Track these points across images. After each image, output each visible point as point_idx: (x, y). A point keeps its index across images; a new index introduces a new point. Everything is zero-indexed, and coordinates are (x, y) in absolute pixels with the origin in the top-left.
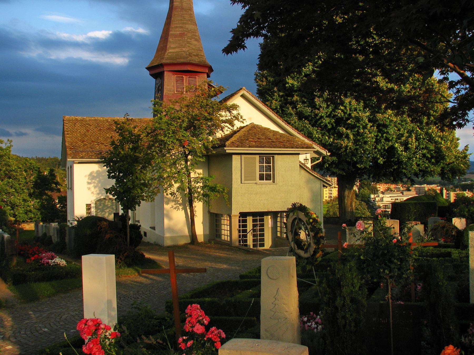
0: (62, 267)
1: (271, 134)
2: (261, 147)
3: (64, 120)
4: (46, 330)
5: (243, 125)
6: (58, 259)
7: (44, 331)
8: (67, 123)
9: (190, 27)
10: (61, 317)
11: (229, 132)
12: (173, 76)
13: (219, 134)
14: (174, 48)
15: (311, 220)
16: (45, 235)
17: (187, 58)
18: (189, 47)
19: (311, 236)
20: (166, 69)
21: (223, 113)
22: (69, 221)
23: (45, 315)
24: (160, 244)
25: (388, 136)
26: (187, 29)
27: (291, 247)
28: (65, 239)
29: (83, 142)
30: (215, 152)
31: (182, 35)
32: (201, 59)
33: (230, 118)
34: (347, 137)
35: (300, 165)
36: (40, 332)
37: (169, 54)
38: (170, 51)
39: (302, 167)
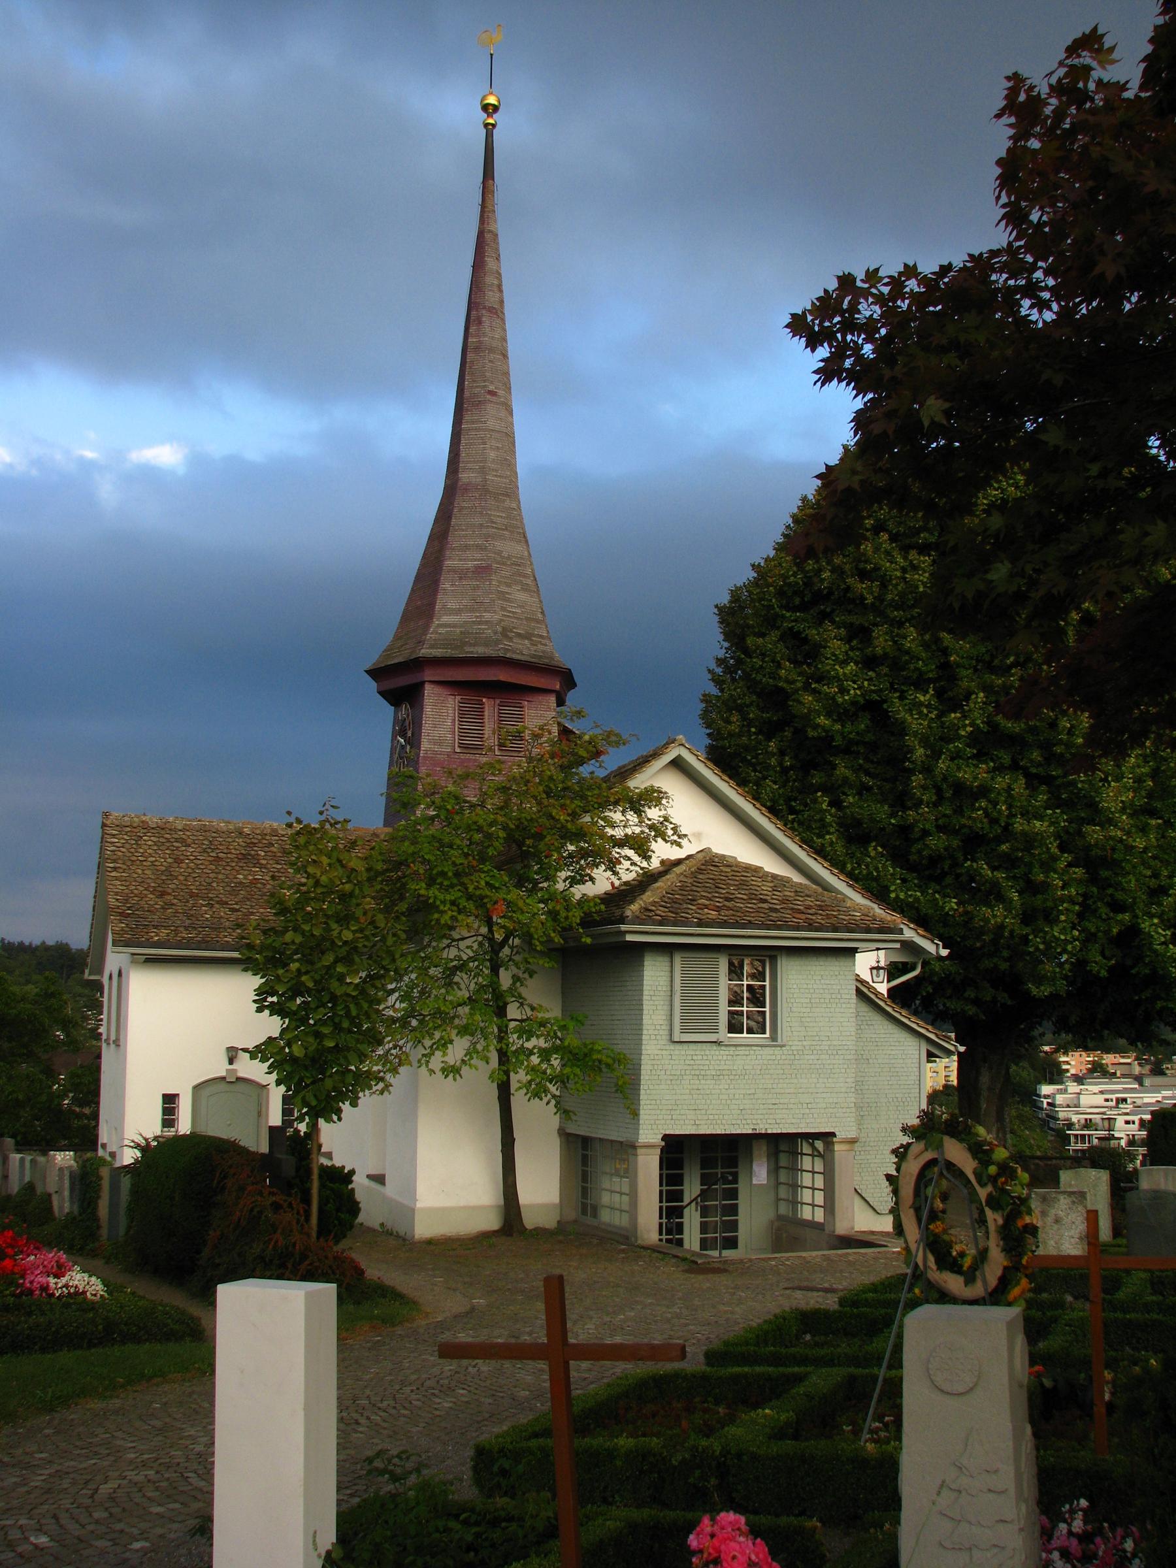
0: (93, 1302)
1: (766, 887)
3: (104, 825)
4: (43, 1540)
5: (674, 853)
6: (79, 1276)
7: (36, 1546)
8: (114, 836)
9: (510, 548)
10: (97, 1489)
11: (633, 876)
13: (602, 882)
14: (458, 612)
15: (993, 1169)
16: (30, 1188)
17: (497, 642)
18: (503, 609)
19: (992, 1227)
20: (429, 674)
21: (617, 816)
22: (104, 1146)
23: (37, 1481)
24: (402, 1234)
25: (1119, 896)
26: (499, 553)
27: (916, 1265)
28: (96, 1205)
29: (162, 894)
30: (589, 940)
31: (482, 571)
33: (637, 830)
34: (1001, 898)
35: (858, 990)
36: (20, 1549)
37: (441, 630)
39: (864, 994)
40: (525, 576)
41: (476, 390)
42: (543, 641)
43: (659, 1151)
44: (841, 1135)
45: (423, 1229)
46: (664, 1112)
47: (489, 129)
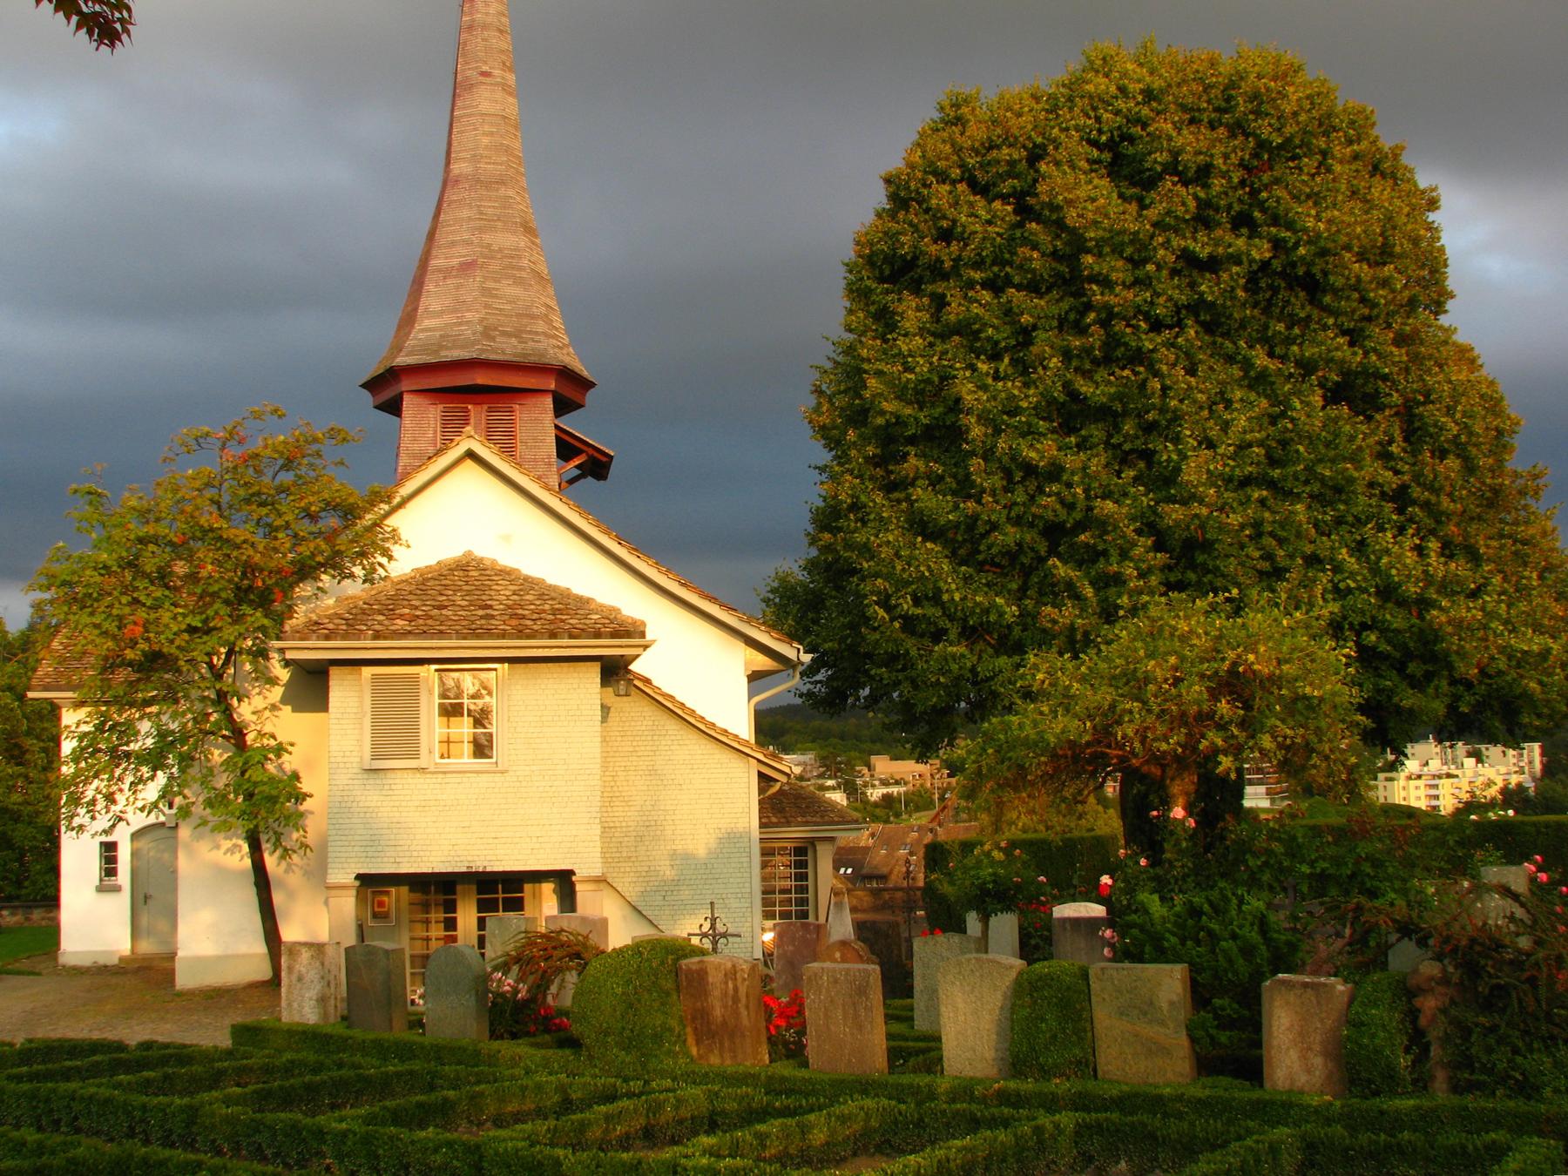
2: (424, 634)
12: (432, 408)
20: (406, 385)
37: (421, 336)
38: (427, 323)
40: (521, 269)
41: (469, 73)
43: (354, 892)
44: (581, 872)
45: (185, 979)
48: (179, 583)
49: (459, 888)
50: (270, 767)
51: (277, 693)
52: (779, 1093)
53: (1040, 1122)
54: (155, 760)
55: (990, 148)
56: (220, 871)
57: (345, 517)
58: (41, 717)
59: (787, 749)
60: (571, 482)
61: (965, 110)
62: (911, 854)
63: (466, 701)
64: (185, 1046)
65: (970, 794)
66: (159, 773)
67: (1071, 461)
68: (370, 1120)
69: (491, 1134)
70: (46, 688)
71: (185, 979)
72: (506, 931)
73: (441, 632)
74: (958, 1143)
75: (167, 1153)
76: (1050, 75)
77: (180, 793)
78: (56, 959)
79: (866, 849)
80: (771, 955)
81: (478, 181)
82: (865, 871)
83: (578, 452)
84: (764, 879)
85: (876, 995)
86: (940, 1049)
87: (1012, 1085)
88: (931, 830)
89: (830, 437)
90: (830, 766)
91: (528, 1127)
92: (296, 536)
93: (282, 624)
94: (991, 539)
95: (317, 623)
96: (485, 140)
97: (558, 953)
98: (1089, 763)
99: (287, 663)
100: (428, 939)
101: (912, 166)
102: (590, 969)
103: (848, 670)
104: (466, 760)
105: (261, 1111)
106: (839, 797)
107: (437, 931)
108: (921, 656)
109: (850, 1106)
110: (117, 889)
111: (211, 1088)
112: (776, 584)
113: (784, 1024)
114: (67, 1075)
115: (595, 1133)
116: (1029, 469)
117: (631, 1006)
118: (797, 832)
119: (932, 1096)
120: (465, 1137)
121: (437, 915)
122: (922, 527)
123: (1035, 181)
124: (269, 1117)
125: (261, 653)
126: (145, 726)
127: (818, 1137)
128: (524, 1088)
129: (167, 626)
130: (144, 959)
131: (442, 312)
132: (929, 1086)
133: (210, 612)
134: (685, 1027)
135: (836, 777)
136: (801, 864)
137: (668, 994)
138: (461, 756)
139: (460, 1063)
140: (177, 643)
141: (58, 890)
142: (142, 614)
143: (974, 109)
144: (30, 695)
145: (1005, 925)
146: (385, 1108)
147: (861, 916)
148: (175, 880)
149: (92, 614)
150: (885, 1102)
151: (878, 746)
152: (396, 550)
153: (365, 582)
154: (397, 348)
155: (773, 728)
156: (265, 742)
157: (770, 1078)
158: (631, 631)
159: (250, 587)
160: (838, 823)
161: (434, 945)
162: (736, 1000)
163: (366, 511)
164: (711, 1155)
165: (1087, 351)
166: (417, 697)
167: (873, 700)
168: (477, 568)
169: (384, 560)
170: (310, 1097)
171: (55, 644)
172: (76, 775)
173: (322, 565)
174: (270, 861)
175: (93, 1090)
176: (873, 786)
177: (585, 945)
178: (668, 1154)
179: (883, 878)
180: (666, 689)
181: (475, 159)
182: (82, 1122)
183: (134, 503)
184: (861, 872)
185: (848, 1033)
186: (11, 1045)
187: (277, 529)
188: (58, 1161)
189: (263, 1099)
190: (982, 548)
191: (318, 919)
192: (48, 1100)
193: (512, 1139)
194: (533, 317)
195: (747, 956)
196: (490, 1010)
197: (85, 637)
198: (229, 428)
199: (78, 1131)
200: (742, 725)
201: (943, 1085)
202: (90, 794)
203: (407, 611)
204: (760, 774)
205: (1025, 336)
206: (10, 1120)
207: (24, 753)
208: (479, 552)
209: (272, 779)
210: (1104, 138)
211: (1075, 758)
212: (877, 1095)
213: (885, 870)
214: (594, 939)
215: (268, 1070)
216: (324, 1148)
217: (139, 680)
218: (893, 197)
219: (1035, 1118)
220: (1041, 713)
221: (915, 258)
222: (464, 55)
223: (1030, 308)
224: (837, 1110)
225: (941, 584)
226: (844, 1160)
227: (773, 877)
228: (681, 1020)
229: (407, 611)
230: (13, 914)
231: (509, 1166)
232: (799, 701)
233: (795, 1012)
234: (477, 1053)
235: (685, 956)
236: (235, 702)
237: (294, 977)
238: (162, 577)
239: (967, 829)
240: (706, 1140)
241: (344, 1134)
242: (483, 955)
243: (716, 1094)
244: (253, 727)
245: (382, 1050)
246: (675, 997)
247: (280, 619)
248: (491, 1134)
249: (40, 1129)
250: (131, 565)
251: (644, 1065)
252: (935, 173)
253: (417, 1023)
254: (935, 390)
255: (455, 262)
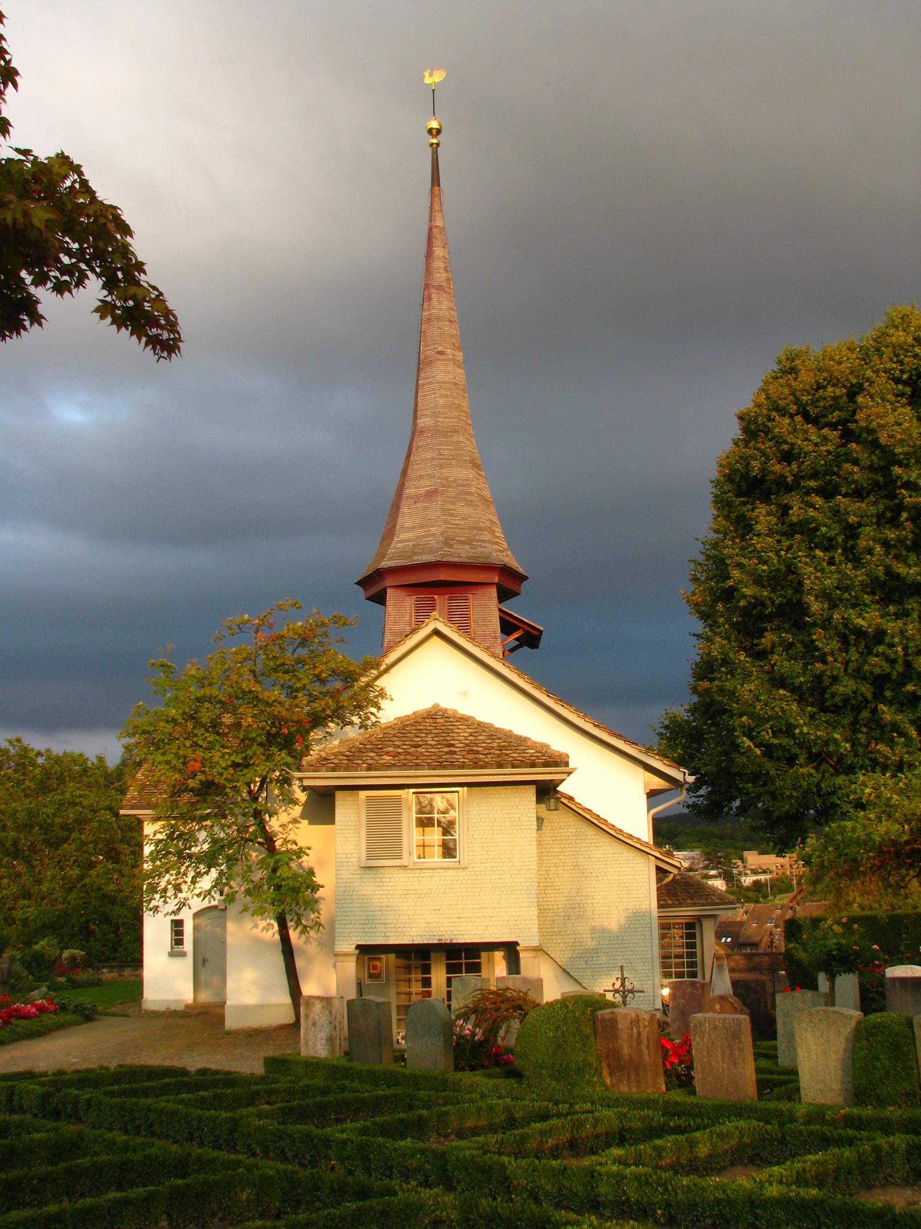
2: (404, 766)
12: (408, 599)
20: (388, 582)
32: (479, 549)
37: (399, 545)
40: (470, 494)
42: (483, 545)
43: (354, 958)
44: (523, 943)
45: (232, 1022)
46: (357, 926)
47: (435, 147)
48: (226, 730)
49: (433, 955)
50: (293, 865)
51: (297, 811)
52: (673, 1115)
53: (877, 1142)
54: (209, 859)
55: (816, 390)
56: (259, 942)
57: (345, 680)
58: (131, 829)
59: (679, 848)
60: (512, 650)
61: (797, 362)
62: (776, 926)
63: (436, 816)
64: (230, 1073)
65: (815, 880)
66: (213, 869)
67: (892, 626)
68: (364, 1132)
69: (454, 1144)
70: (133, 807)
71: (232, 1022)
72: (467, 989)
73: (417, 764)
74: (812, 1157)
75: (215, 1153)
76: (863, 335)
77: (227, 884)
78: (140, 1005)
79: (742, 923)
80: (668, 1006)
81: (438, 431)
82: (741, 940)
83: (517, 628)
84: (663, 947)
85: (747, 1038)
86: (798, 1081)
87: (855, 1111)
88: (791, 908)
89: (707, 616)
90: (712, 860)
91: (481, 1139)
92: (310, 695)
93: (301, 760)
94: (833, 689)
95: (325, 759)
96: (442, 401)
97: (504, 1006)
98: (909, 857)
99: (304, 789)
100: (410, 994)
101: (759, 406)
102: (529, 1018)
103: (723, 789)
104: (436, 860)
105: (284, 1123)
106: (719, 884)
107: (416, 988)
108: (778, 775)
109: (728, 1126)
110: (183, 954)
111: (248, 1105)
112: (667, 722)
113: (677, 1061)
114: (145, 1093)
115: (532, 1144)
116: (859, 633)
117: (559, 1046)
118: (688, 912)
119: (792, 1119)
120: (434, 1146)
121: (417, 976)
122: (778, 681)
123: (854, 412)
124: (290, 1128)
125: (286, 781)
126: (202, 835)
127: (703, 1150)
128: (479, 1109)
129: (217, 763)
130: (202, 1007)
131: (414, 527)
132: (789, 1110)
133: (249, 752)
134: (600, 1062)
135: (717, 868)
136: (691, 936)
137: (587, 1037)
138: (433, 856)
139: (431, 1089)
140: (225, 775)
141: (142, 954)
142: (200, 753)
143: (803, 361)
144: (122, 812)
145: (848, 984)
146: (374, 1123)
147: (737, 975)
148: (226, 948)
149: (164, 754)
150: (754, 1123)
151: (749, 844)
152: (383, 703)
153: (360, 728)
154: (382, 555)
155: (666, 831)
156: (289, 846)
157: (666, 1103)
158: (558, 762)
159: (277, 733)
160: (718, 904)
161: (415, 998)
162: (639, 1042)
163: (361, 675)
164: (620, 1163)
165: (901, 541)
166: (399, 812)
167: (742, 810)
168: (443, 717)
169: (374, 710)
170: (320, 1113)
171: (139, 775)
172: (153, 871)
173: (330, 716)
174: (293, 935)
175: (163, 1104)
176: (746, 875)
177: (525, 1000)
178: (586, 1162)
179: (755, 945)
180: (585, 805)
181: (435, 415)
182: (156, 1128)
183: (193, 672)
184: (739, 942)
185: (726, 1065)
186: (107, 1069)
187: (297, 690)
188: (138, 1157)
189: (286, 1115)
190: (827, 696)
191: (328, 979)
192: (132, 1111)
193: (469, 1148)
194: (480, 529)
195: (649, 1008)
196: (455, 1049)
197: (157, 771)
198: (262, 617)
199: (153, 1134)
200: (643, 831)
201: (801, 1110)
202: (163, 884)
203: (391, 749)
204: (658, 868)
205: (852, 532)
206: (106, 1124)
207: (119, 854)
208: (444, 705)
209: (295, 876)
210: (905, 376)
211: (898, 854)
212: (749, 1118)
213: (756, 939)
214: (532, 995)
215: (291, 1092)
216: (330, 1153)
217: (198, 801)
218: (746, 430)
219: (874, 1139)
220: (869, 819)
221: (763, 476)
222: (425, 340)
223: (854, 510)
224: (718, 1128)
225: (792, 720)
226: (724, 1168)
227: (669, 946)
228: (598, 1058)
229: (391, 749)
230: (110, 972)
231: (468, 1169)
232: (686, 811)
233: (685, 1050)
234: (445, 1081)
235: (601, 1008)
236: (267, 817)
237: (310, 1022)
238: (215, 727)
239: (819, 907)
240: (617, 1152)
241: (345, 1142)
242: (449, 1006)
243: (625, 1115)
244: (280, 836)
245: (375, 1078)
246: (593, 1039)
247: (298, 757)
248: (454, 1144)
249: (126, 1132)
250: (192, 717)
251: (570, 1092)
252: (778, 409)
253: (400, 1057)
254: (786, 577)
255: (423, 490)
